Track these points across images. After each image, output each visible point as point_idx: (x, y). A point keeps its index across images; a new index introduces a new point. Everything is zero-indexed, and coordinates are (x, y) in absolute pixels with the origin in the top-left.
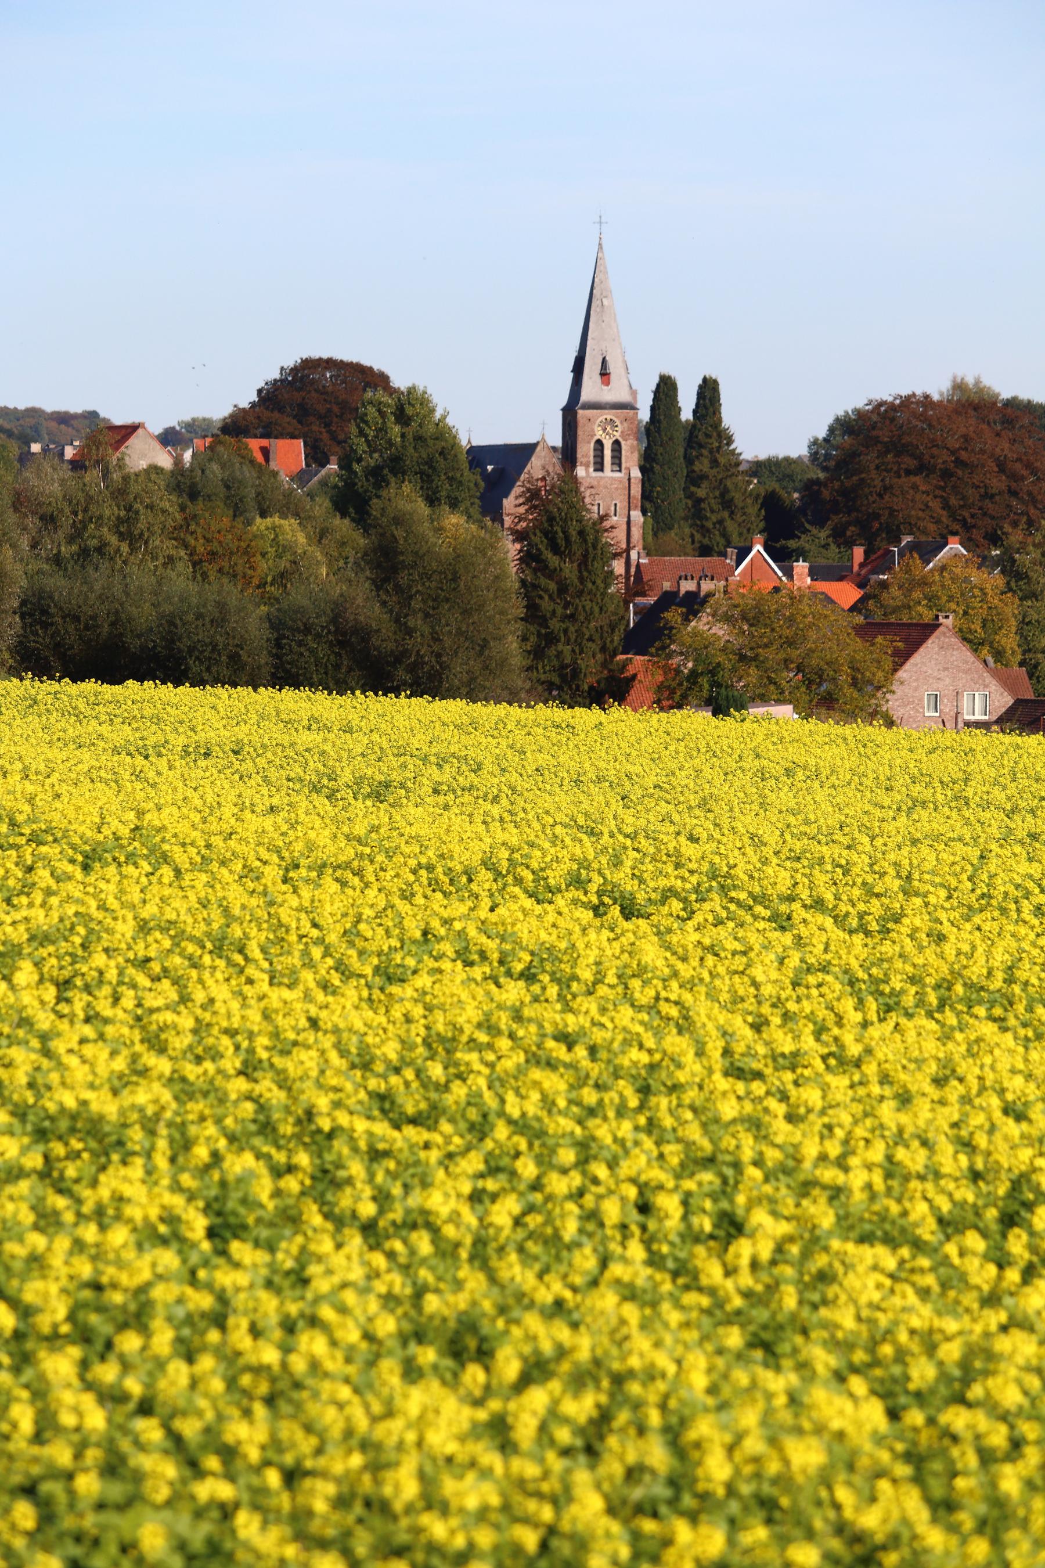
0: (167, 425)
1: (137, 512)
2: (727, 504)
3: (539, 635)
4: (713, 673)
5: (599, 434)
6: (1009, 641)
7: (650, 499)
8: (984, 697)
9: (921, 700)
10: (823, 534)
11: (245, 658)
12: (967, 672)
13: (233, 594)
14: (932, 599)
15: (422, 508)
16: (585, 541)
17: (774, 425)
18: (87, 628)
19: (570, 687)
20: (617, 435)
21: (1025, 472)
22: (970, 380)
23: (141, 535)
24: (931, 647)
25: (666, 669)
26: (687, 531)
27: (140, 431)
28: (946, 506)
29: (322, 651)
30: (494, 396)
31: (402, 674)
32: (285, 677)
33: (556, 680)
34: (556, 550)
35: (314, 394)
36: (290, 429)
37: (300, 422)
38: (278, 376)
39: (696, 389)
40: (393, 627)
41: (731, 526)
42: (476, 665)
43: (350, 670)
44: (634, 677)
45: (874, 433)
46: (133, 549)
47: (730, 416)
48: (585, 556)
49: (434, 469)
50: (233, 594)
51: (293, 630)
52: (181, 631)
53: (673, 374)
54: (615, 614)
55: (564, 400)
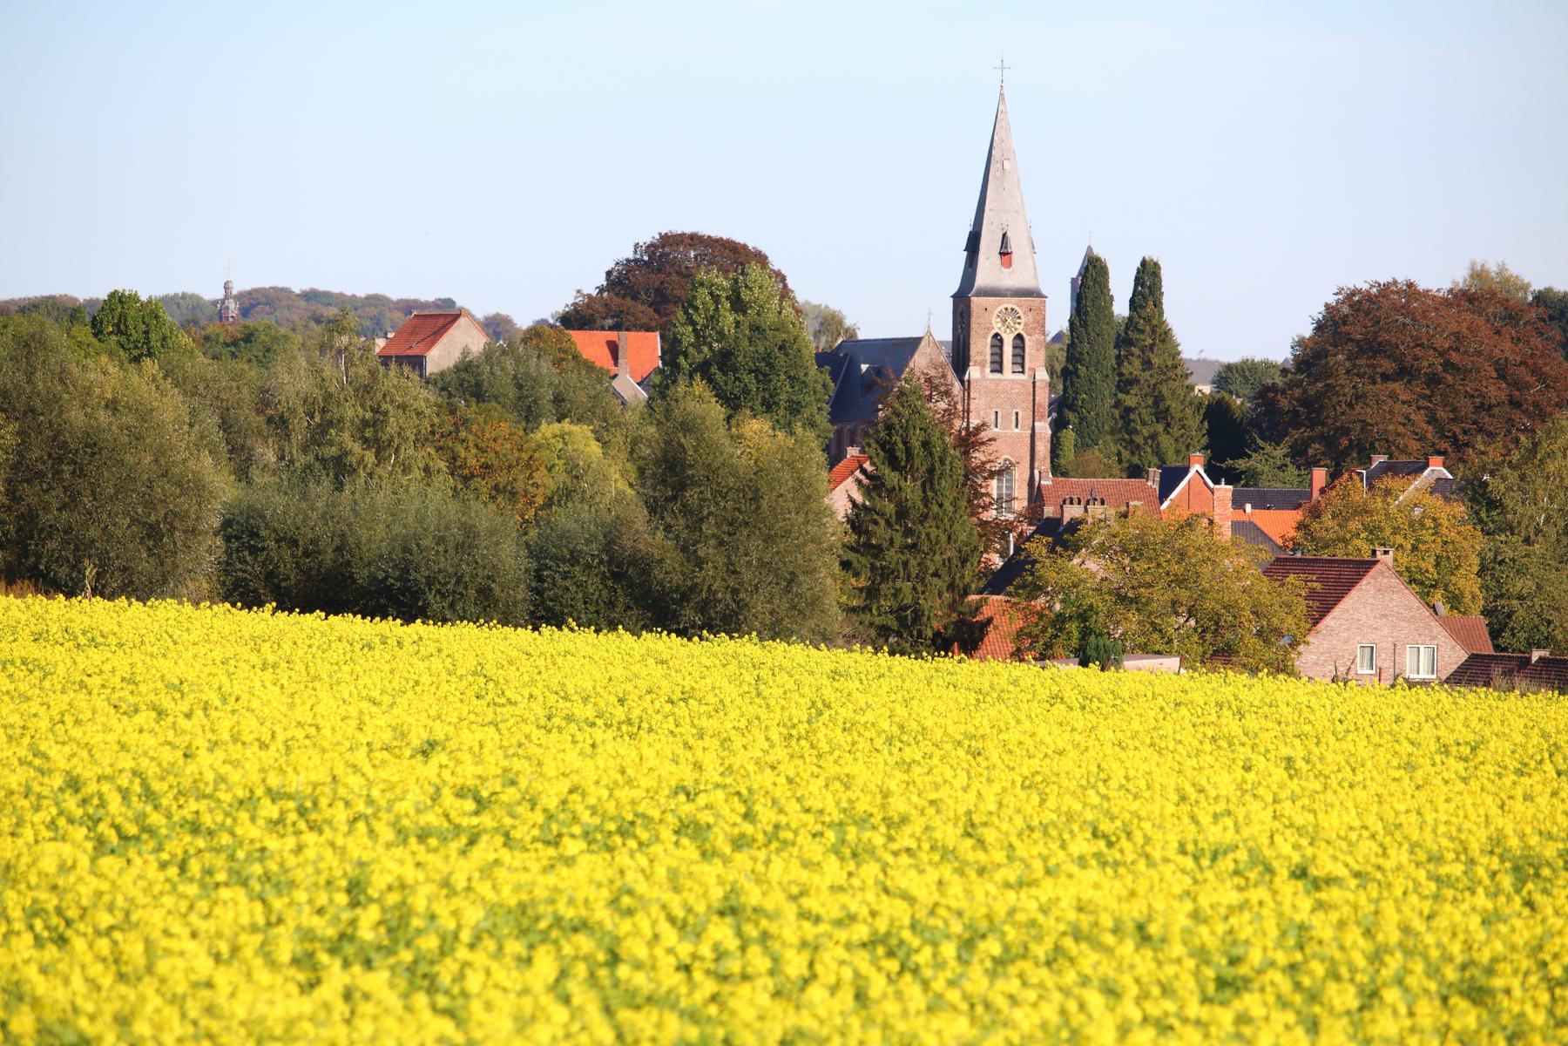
0: (539, 318)
1: (386, 414)
2: (1162, 415)
3: (873, 568)
4: (1083, 617)
5: (997, 327)
6: (1468, 583)
7: (1063, 410)
8: (1431, 648)
10: (1280, 452)
13: (484, 514)
14: (1373, 531)
15: (717, 411)
16: (931, 454)
17: (1239, 318)
18: (306, 554)
19: (905, 633)
21: (1531, 379)
22: (1493, 268)
23: (391, 440)
24: (1366, 586)
25: (1028, 613)
26: (1114, 448)
27: (462, 320)
28: (1432, 420)
29: (594, 585)
30: (869, 277)
31: (689, 614)
32: (545, 613)
33: (895, 625)
35: (675, 277)
36: (645, 320)
37: (657, 311)
38: (631, 256)
41: (1166, 442)
42: (782, 604)
43: (628, 608)
44: (990, 621)
45: (1345, 329)
46: (380, 460)
47: (1176, 311)
48: (931, 471)
50: (484, 514)
51: (555, 558)
52: (416, 558)
55: (955, 288)
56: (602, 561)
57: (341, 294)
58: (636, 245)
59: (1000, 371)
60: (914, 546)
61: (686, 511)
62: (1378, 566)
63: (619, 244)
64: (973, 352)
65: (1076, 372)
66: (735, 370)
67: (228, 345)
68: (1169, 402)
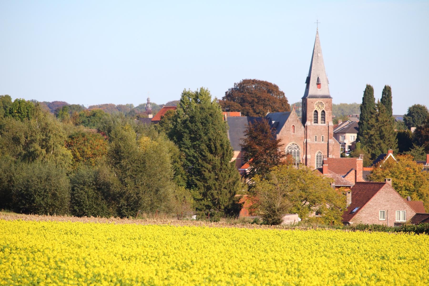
1: (50, 137)
2: (382, 137)
5: (316, 108)
9: (378, 214)
10: (421, 149)
11: (58, 195)
12: (397, 202)
16: (223, 148)
17: (218, 99)
20: (324, 109)
23: (51, 146)
29: (91, 192)
33: (211, 204)
34: (211, 152)
36: (237, 108)
37: (241, 105)
38: (233, 87)
39: (382, 90)
40: (119, 182)
48: (223, 154)
49: (207, 121)
51: (78, 183)
53: (371, 85)
54: (235, 178)
55: (302, 95)
56: (93, 184)
58: (235, 84)
59: (317, 123)
60: (218, 179)
61: (121, 166)
62: (386, 185)
64: (308, 117)
65: (362, 123)
66: (195, 123)
67: (88, 117)
68: (384, 133)
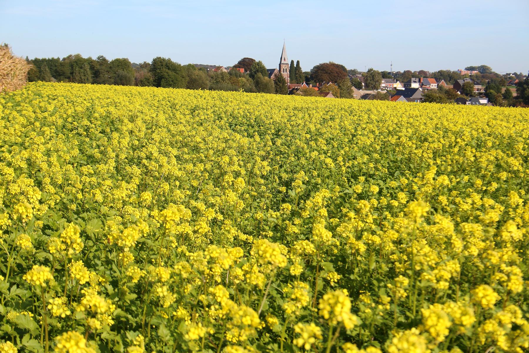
2: (300, 77)
17: (306, 67)
30: (270, 63)
57: (53, 59)
63: (240, 59)
